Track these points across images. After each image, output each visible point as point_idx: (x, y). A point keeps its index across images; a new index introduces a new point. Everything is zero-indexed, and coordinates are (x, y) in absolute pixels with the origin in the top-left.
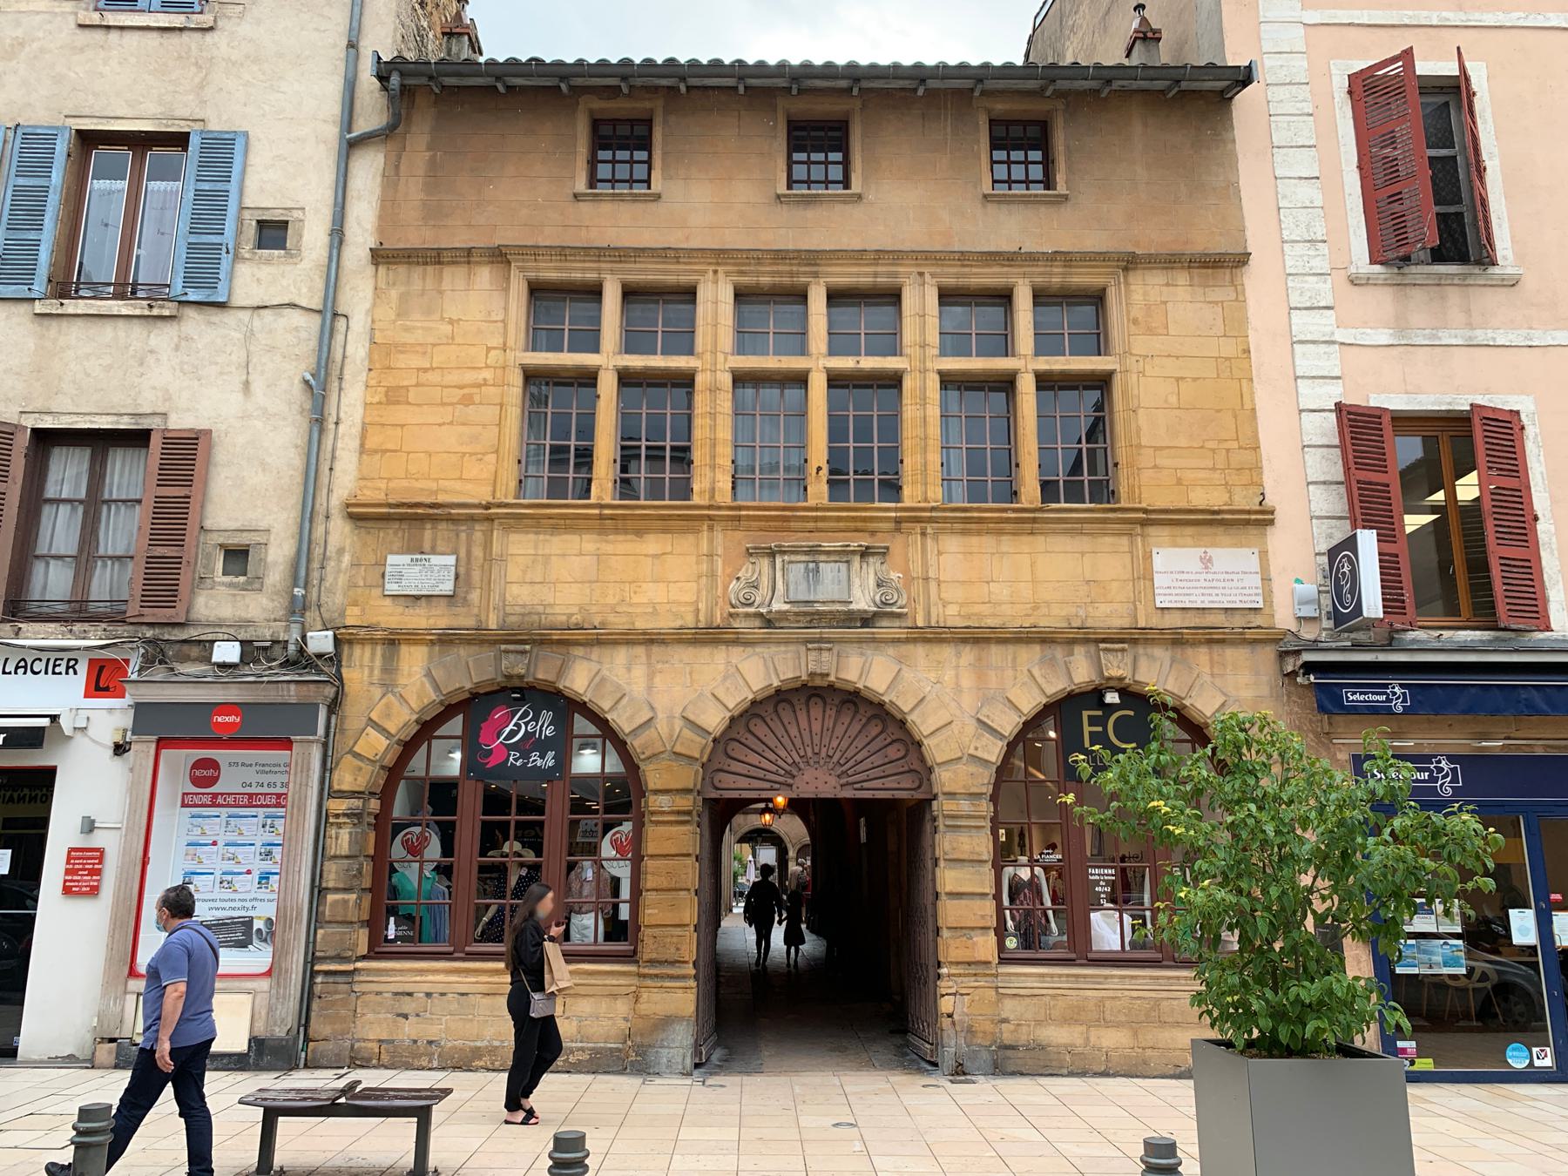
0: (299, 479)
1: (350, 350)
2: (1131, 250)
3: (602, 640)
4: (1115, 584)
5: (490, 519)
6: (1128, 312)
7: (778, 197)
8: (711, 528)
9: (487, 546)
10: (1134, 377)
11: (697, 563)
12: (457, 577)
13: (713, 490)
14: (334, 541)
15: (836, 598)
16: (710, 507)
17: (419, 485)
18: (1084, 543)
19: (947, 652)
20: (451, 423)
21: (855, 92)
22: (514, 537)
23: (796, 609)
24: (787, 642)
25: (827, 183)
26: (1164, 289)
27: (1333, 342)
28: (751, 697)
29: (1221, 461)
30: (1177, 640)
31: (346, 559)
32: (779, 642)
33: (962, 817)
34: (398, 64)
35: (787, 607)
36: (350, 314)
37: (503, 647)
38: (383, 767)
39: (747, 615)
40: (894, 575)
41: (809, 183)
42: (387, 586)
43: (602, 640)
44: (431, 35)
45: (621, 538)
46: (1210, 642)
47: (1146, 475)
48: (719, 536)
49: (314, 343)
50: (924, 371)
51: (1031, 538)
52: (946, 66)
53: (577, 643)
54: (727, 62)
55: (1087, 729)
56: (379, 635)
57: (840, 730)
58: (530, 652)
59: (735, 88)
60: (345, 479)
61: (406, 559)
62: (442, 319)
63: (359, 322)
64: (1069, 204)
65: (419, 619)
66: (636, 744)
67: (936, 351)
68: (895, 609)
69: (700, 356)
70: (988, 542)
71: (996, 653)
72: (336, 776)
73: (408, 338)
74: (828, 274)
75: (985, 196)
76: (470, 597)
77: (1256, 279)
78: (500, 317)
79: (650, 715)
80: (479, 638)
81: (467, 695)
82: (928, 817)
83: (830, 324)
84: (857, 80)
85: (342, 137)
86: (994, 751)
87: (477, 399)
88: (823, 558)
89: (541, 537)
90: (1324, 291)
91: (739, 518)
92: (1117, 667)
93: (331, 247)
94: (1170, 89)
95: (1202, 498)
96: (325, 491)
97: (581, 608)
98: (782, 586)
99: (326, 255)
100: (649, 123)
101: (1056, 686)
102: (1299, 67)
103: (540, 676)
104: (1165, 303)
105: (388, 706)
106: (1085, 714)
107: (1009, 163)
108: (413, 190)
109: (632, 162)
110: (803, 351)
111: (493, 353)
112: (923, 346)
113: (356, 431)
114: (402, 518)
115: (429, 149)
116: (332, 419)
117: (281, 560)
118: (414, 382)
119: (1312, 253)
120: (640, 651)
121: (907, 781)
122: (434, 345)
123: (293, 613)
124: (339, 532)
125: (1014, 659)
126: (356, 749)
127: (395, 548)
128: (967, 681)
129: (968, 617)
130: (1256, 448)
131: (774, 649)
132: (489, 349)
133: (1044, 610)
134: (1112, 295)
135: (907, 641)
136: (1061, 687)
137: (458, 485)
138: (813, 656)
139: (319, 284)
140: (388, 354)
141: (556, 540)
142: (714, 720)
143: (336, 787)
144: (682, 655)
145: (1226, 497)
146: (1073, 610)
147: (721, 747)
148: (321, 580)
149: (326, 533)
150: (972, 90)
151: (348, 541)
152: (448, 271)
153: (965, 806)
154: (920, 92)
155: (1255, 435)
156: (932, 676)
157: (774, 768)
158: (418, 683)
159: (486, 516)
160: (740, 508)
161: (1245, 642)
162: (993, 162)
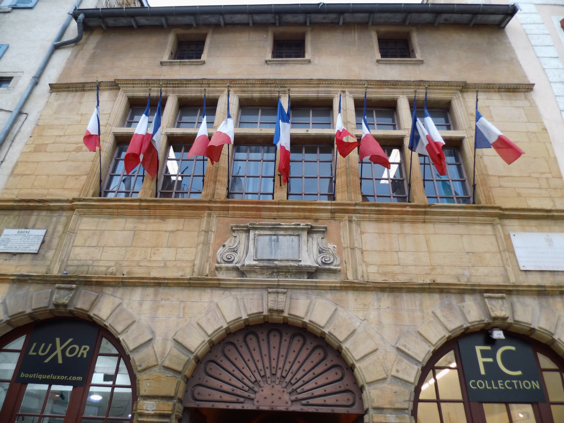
1: (23, 128)
4: (488, 256)
6: (467, 111)
8: (209, 215)
9: (66, 225)
11: (198, 236)
13: (214, 194)
15: (290, 257)
16: (210, 202)
18: (460, 229)
19: (370, 298)
20: (66, 160)
22: (85, 220)
23: (261, 264)
28: (225, 326)
30: (541, 292)
39: (228, 269)
40: (331, 246)
45: (152, 221)
48: (214, 220)
51: (423, 225)
55: (481, 360)
61: (15, 231)
62: (78, 114)
68: (332, 267)
70: (395, 227)
71: (408, 302)
76: (46, 255)
79: (150, 337)
80: (45, 280)
88: (282, 233)
89: (102, 220)
91: (227, 209)
92: (499, 309)
95: (534, 204)
97: (117, 263)
98: (251, 249)
101: (455, 324)
103: (79, 306)
104: (488, 107)
118: (52, 142)
120: (150, 291)
121: (343, 399)
122: (69, 125)
125: (421, 305)
127: (11, 225)
128: (387, 320)
129: (385, 274)
131: (245, 292)
133: (439, 270)
136: (415, 371)
138: (272, 297)
142: (196, 342)
144: (177, 296)
146: (460, 271)
147: (202, 366)
155: (559, 171)
156: (361, 315)
157: (240, 385)
159: (71, 207)
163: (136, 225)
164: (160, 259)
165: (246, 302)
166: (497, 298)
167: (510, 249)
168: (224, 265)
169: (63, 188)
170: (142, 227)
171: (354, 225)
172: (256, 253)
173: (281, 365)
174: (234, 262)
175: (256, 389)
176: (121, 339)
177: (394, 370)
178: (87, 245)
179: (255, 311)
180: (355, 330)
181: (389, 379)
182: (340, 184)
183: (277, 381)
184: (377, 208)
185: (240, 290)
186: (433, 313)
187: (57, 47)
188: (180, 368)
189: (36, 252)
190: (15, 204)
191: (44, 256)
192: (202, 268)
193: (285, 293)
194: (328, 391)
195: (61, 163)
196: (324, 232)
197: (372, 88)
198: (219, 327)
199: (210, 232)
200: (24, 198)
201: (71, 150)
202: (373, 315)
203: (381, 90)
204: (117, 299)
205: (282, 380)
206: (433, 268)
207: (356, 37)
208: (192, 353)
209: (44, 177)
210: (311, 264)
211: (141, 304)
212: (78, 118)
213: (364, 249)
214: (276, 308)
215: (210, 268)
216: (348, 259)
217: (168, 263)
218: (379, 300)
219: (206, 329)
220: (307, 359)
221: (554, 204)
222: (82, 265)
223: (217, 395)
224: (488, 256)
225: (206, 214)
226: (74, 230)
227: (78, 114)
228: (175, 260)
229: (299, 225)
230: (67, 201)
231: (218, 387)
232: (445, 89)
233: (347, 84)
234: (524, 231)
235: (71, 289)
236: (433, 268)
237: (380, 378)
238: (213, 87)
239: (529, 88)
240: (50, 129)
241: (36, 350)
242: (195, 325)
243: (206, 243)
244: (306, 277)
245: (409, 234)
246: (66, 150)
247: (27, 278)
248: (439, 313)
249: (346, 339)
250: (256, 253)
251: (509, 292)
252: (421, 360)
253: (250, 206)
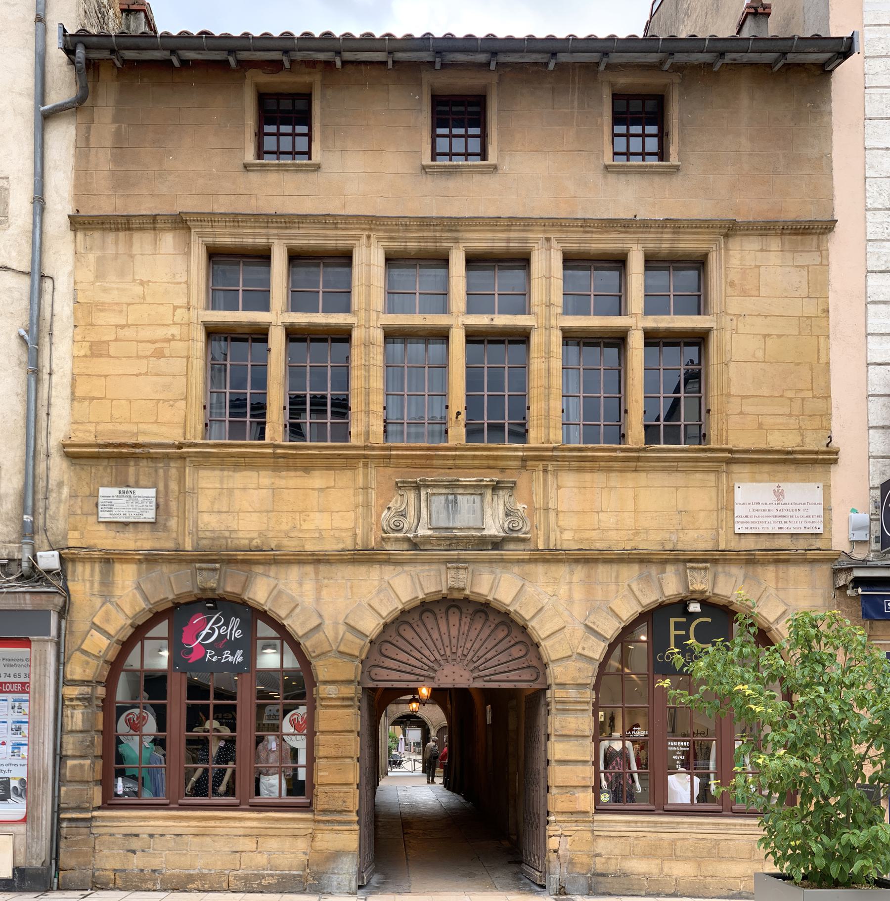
8: (366, 465)
11: (355, 495)
15: (471, 525)
16: (365, 448)
18: (678, 479)
19: (562, 570)
20: (146, 374)
22: (203, 473)
23: (437, 535)
35: (430, 533)
37: (198, 565)
39: (397, 539)
40: (520, 506)
42: (101, 514)
45: (292, 474)
48: (372, 472)
51: (634, 475)
55: (673, 633)
58: (220, 569)
61: (115, 491)
62: (134, 280)
66: (308, 645)
68: (520, 535)
70: (599, 478)
71: (603, 572)
72: (68, 669)
79: (315, 622)
80: (178, 558)
86: (597, 650)
87: (167, 352)
88: (461, 491)
92: (700, 582)
97: (261, 533)
98: (425, 516)
101: (650, 598)
103: (229, 589)
106: (672, 621)
111: (178, 311)
113: (67, 380)
118: (113, 338)
120: (309, 569)
121: (526, 675)
122: (129, 304)
125: (617, 577)
126: (84, 647)
127: (105, 481)
128: (578, 595)
129: (581, 541)
131: (419, 568)
132: (175, 308)
133: (643, 536)
138: (451, 573)
142: (371, 625)
156: (550, 590)
157: (419, 664)
163: (273, 480)
164: (313, 527)
165: (422, 579)
166: (700, 569)
169: (156, 422)
170: (282, 483)
174: (404, 530)
175: (436, 668)
177: (580, 647)
178: (216, 510)
181: (574, 657)
182: (535, 414)
184: (579, 454)
185: (414, 565)
190: (101, 450)
192: (366, 539)
193: (466, 568)
196: (512, 487)
197: (592, 232)
199: (370, 490)
201: (149, 354)
202: (563, 590)
207: (576, 104)
208: (367, 636)
210: (496, 533)
211: (301, 585)
212: (138, 289)
214: (456, 586)
216: (540, 524)
218: (572, 573)
221: (802, 440)
222: (218, 538)
223: (395, 675)
225: (361, 464)
226: (193, 489)
228: (332, 529)
236: (637, 533)
238: (342, 229)
240: (101, 311)
242: (366, 605)
248: (635, 587)
253: (418, 453)
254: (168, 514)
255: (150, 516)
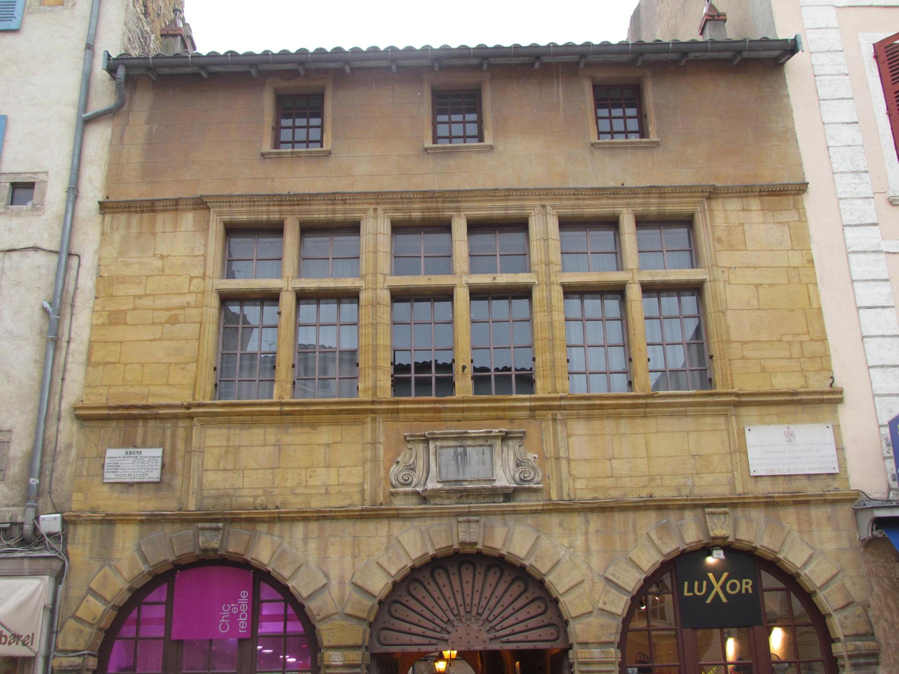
0: (37, 388)
1: (81, 282)
2: (712, 183)
3: (281, 518)
4: (716, 458)
5: (191, 417)
6: (713, 234)
7: (426, 150)
8: (374, 420)
9: (188, 440)
10: (722, 285)
11: (363, 450)
12: (163, 466)
14: (63, 439)
16: (373, 402)
17: (132, 390)
18: (688, 423)
19: (576, 521)
20: (161, 339)
21: (485, 67)
22: (211, 432)
23: (447, 487)
24: (440, 515)
25: (465, 138)
26: (741, 213)
27: (881, 252)
28: (410, 564)
29: (796, 352)
30: (770, 503)
31: (74, 452)
32: (433, 516)
33: (594, 663)
34: (124, 59)
35: (439, 486)
36: (81, 255)
37: (200, 525)
38: (100, 629)
39: (406, 494)
40: (530, 456)
41: (450, 138)
42: (106, 475)
43: (281, 518)
44: (153, 37)
45: (299, 430)
46: (797, 503)
47: (737, 364)
48: (381, 426)
49: (51, 278)
50: (549, 284)
51: (644, 421)
52: (555, 46)
53: (262, 521)
54: (382, 49)
56: (98, 516)
57: (488, 591)
58: (223, 529)
59: (389, 68)
60: (74, 389)
61: (122, 452)
63: (89, 260)
64: (332, 156)
65: (132, 504)
66: (313, 606)
67: (559, 268)
69: (363, 277)
70: (609, 425)
73: (128, 272)
74: (470, 209)
75: (593, 145)
77: (811, 202)
78: (201, 252)
79: (324, 581)
80: (184, 519)
81: (171, 567)
82: (565, 664)
83: (471, 247)
84: (486, 58)
85: (79, 116)
86: (619, 604)
87: (181, 318)
88: (469, 442)
89: (232, 431)
90: (869, 211)
91: (397, 411)
92: (720, 528)
93: (68, 201)
94: (734, 57)
95: (782, 383)
96: (57, 397)
98: (433, 469)
99: (63, 208)
100: (321, 97)
101: (670, 546)
102: (834, 39)
103: (231, 550)
104: (742, 224)
105: (105, 577)
107: (610, 118)
108: (134, 154)
109: (308, 127)
110: (450, 271)
111: (195, 281)
112: (548, 264)
113: (84, 348)
114: (119, 418)
115: (147, 123)
116: (65, 338)
117: (20, 454)
118: (131, 306)
119: (857, 181)
120: (314, 526)
122: (148, 276)
123: (28, 499)
124: (67, 430)
126: (78, 614)
129: (595, 489)
130: (824, 340)
131: (429, 522)
133: (658, 481)
134: (699, 218)
135: (543, 511)
137: (165, 390)
138: (462, 527)
139: (58, 231)
140: (111, 285)
141: (245, 433)
142: (379, 584)
143: (60, 647)
145: (802, 381)
146: (681, 481)
147: (386, 608)
148: (52, 471)
149: (58, 432)
150: (578, 63)
151: (75, 439)
152: (160, 217)
153: (596, 653)
154: (537, 66)
156: (565, 542)
158: (128, 558)
159: (187, 414)
160: (398, 402)
161: (825, 502)
162: (598, 118)
164: (318, 483)
166: (720, 514)
167: (743, 450)
168: (400, 489)
169: (167, 384)
170: (288, 439)
171: (559, 427)
172: (440, 472)
173: (476, 601)
174: (413, 484)
175: (450, 629)
176: (290, 585)
177: (601, 602)
178: (221, 468)
179: (444, 545)
180: (558, 562)
181: (595, 612)
183: (473, 620)
184: (587, 402)
186: (647, 534)
187: (87, 121)
188: (364, 615)
189: (158, 480)
191: (169, 485)
192: (375, 494)
193: (477, 521)
194: (530, 627)
195: (154, 342)
197: (584, 199)
198: (403, 565)
199: (378, 445)
200: (121, 404)
201: (163, 320)
203: (597, 202)
204: (275, 538)
205: (478, 617)
206: (652, 479)
207: (561, 94)
209: (136, 366)
210: (507, 485)
212: (158, 263)
213: (571, 458)
214: (468, 540)
215: (384, 494)
216: (552, 473)
217: (330, 489)
219: (388, 569)
220: (505, 592)
224: (716, 458)
227: (155, 255)
228: (339, 485)
229: (491, 432)
230: (181, 406)
231: (407, 630)
232: (687, 197)
233: (547, 194)
234: (763, 423)
235: (217, 529)
237: (586, 611)
238: (350, 204)
239: (801, 188)
240: (122, 283)
241: (691, 589)
242: (375, 565)
243: (375, 459)
244: (501, 499)
245: (626, 434)
246: (156, 320)
247: (159, 518)
248: (654, 536)
249: (549, 572)
250: (440, 472)
251: (734, 505)
252: (630, 590)
254: (173, 472)
255: (155, 475)
